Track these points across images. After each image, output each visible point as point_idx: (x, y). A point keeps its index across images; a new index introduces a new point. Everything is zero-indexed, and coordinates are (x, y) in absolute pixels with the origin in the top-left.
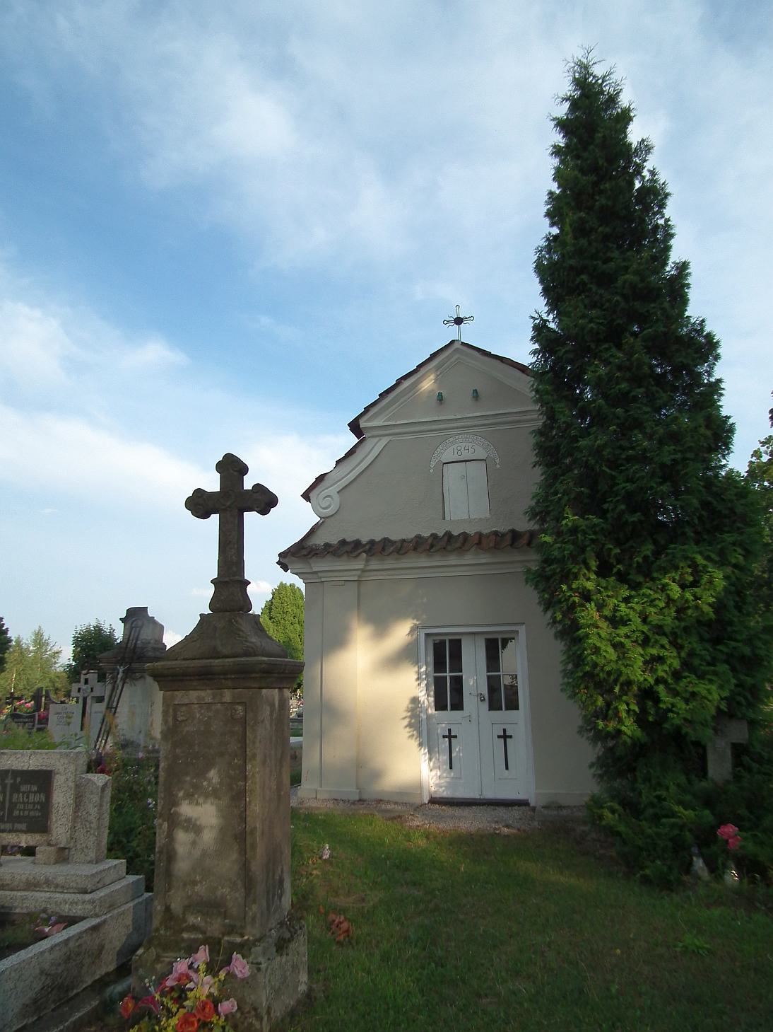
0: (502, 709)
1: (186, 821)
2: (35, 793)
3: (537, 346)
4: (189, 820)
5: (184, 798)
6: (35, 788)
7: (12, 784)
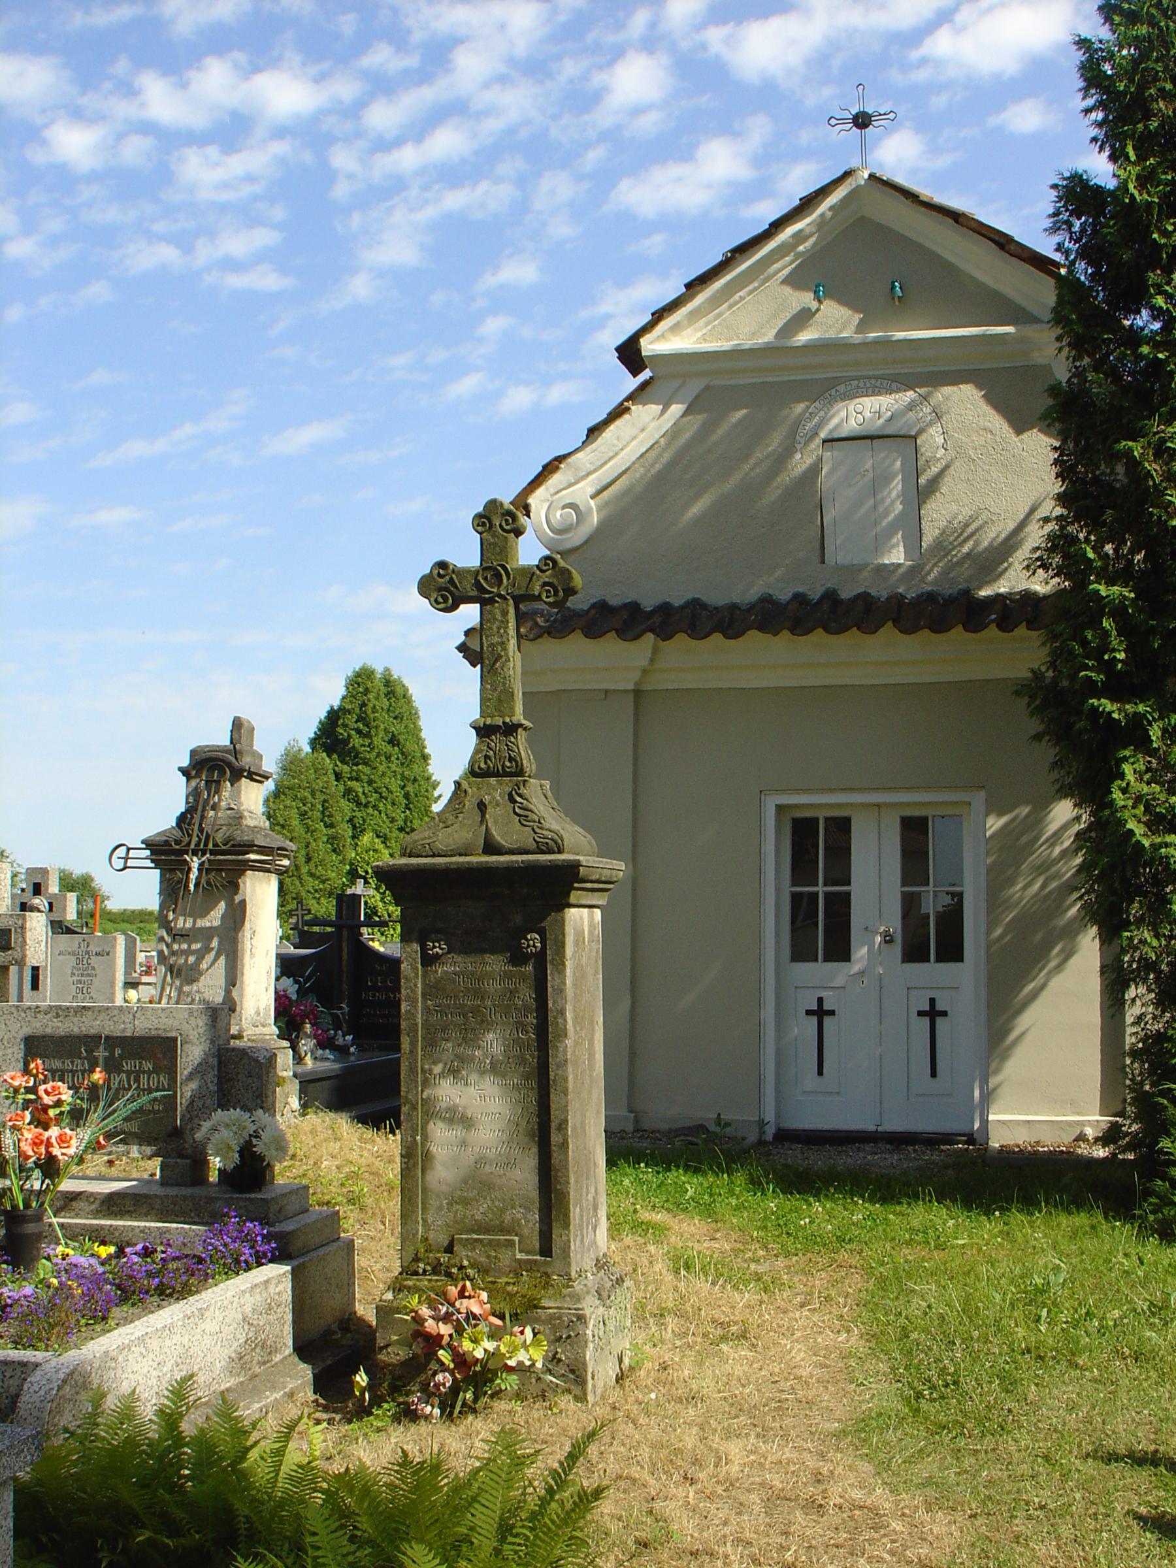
0: (928, 961)
1: (448, 1110)
2: (150, 1073)
3: (1059, 331)
4: (452, 1110)
5: (442, 1075)
6: (148, 1066)
7: (105, 1058)
